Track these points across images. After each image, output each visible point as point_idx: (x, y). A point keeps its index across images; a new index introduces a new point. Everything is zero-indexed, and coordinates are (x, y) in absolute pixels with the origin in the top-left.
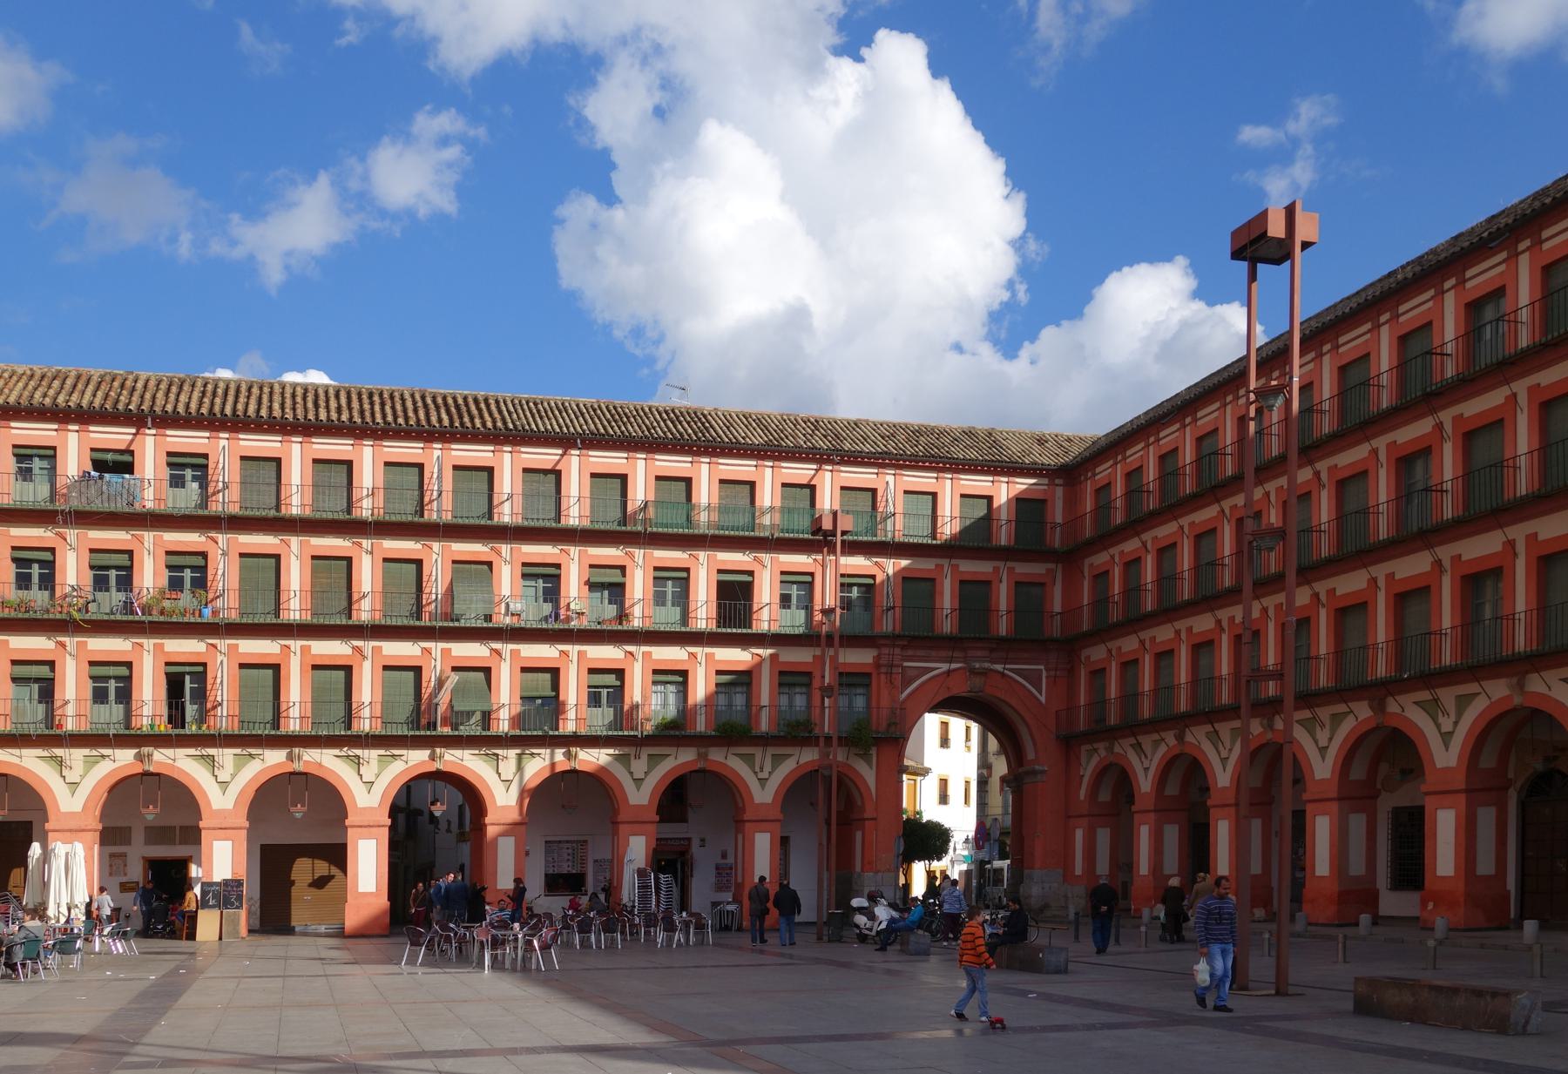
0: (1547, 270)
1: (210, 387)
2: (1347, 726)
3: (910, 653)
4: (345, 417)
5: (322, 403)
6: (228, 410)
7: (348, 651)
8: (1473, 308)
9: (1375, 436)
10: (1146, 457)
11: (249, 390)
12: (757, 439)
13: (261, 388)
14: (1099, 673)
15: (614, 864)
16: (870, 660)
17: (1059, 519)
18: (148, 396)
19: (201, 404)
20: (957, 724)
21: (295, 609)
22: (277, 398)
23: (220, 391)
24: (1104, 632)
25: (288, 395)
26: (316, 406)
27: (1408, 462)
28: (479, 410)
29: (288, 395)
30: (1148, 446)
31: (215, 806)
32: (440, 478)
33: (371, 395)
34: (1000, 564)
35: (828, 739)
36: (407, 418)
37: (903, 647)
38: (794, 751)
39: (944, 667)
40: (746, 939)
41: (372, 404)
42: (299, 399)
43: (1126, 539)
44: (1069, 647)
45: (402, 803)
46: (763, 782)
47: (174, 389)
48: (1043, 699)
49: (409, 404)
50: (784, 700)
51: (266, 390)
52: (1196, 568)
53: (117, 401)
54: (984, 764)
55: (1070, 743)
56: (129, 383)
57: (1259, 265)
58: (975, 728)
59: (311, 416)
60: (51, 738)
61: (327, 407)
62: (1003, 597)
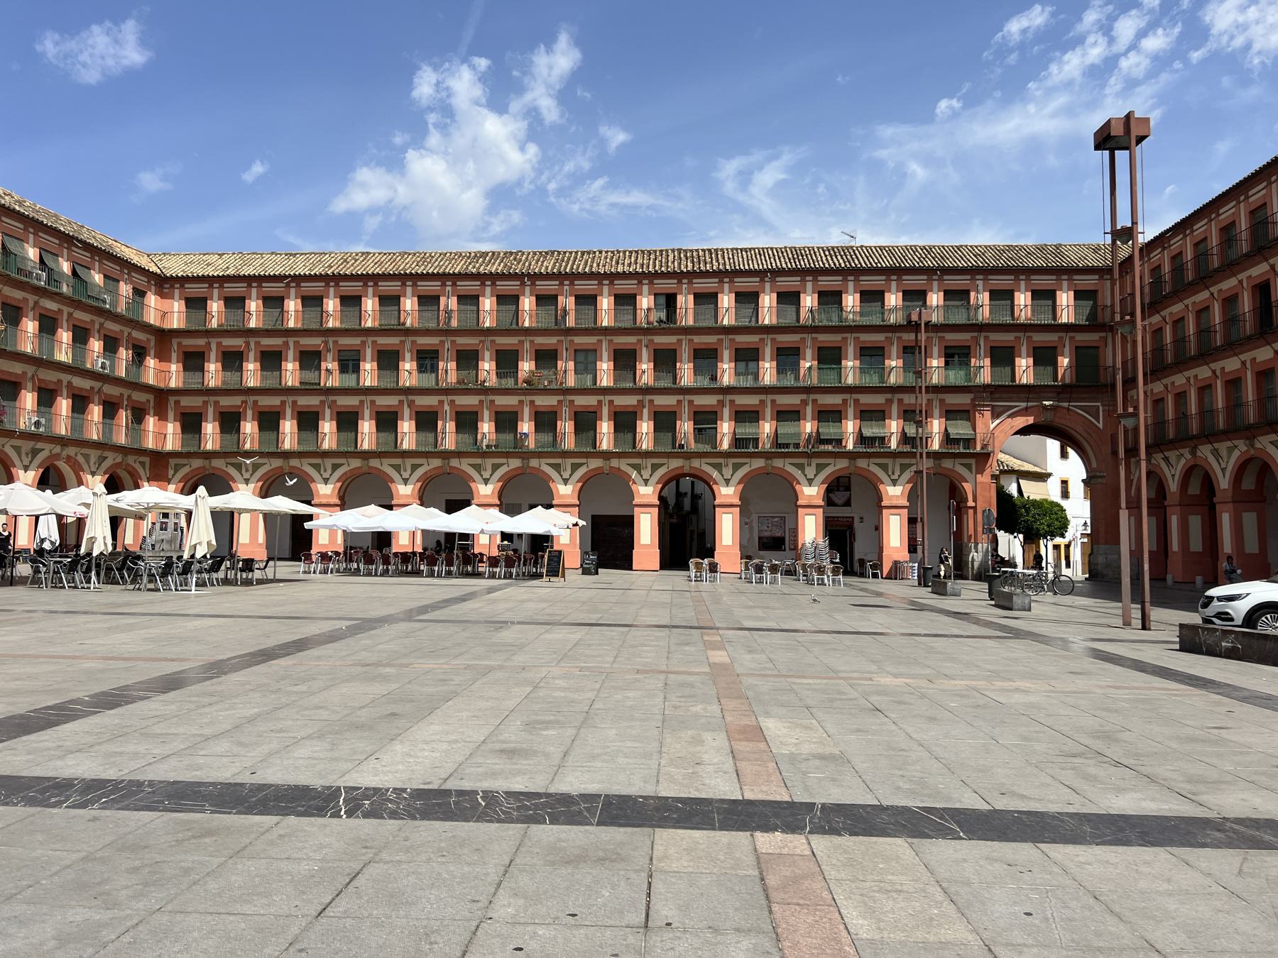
0: (1252, 213)
16: (969, 401)
27: (1230, 301)
30: (1185, 236)
39: (1024, 405)
40: (908, 589)
43: (1198, 292)
48: (1101, 426)
52: (1175, 342)
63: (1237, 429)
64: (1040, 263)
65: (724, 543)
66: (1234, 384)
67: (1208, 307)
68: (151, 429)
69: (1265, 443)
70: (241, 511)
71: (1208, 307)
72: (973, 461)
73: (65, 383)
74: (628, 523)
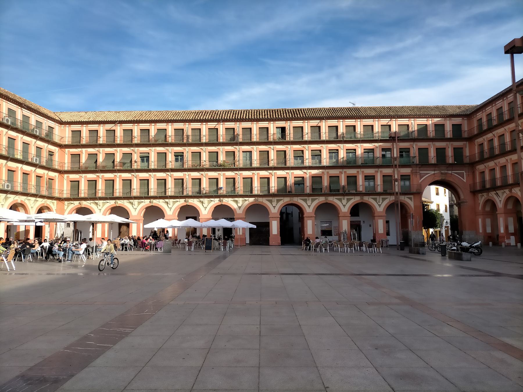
6: (239, 117)
7: (234, 174)
10: (493, 110)
12: (373, 114)
14: (483, 173)
15: (339, 227)
20: (441, 189)
22: (250, 113)
24: (483, 160)
28: (299, 112)
31: (238, 212)
32: (290, 130)
33: (272, 111)
34: (448, 143)
35: (397, 193)
36: (281, 116)
37: (419, 167)
38: (389, 197)
39: (433, 172)
41: (273, 113)
44: (472, 165)
45: (284, 211)
46: (380, 205)
48: (465, 181)
50: (367, 183)
54: (451, 200)
55: (474, 192)
57: (515, 55)
58: (447, 190)
60: (164, 197)
63: (505, 186)
65: (382, 220)
66: (492, 170)
67: (503, 135)
68: (57, 188)
69: (517, 192)
70: (97, 222)
71: (503, 135)
73: (19, 168)
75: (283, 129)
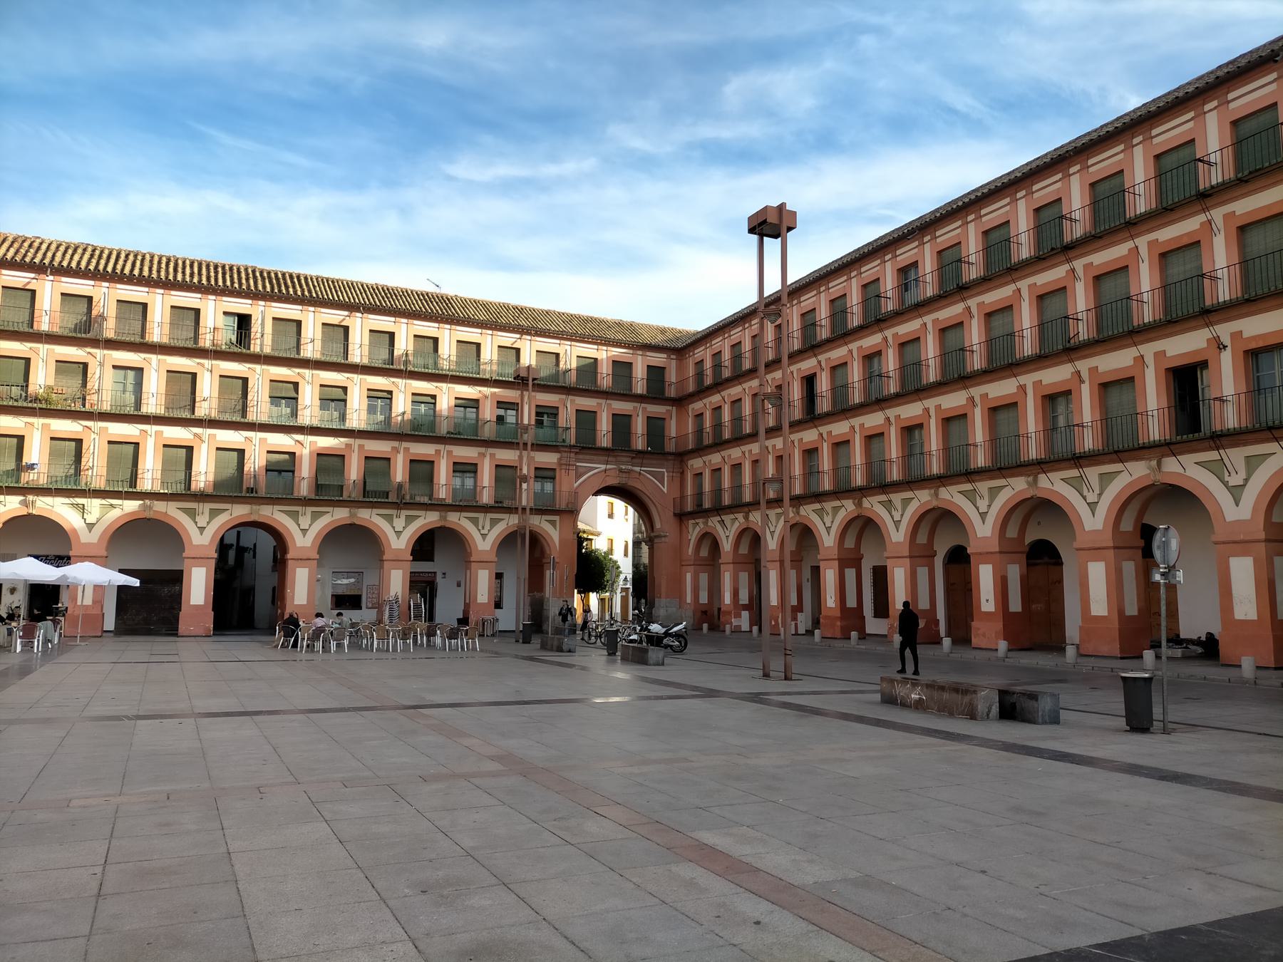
1: (97, 253)
2: (842, 514)
3: (581, 457)
4: (195, 280)
5: (180, 270)
8: (904, 271)
9: (851, 342)
10: (723, 345)
11: (127, 256)
12: (482, 316)
13: (136, 256)
14: (699, 475)
17: (674, 380)
18: (49, 255)
19: (89, 263)
20: (619, 505)
21: (152, 405)
23: (105, 256)
25: (156, 262)
26: (175, 270)
27: (871, 358)
29: (156, 262)
33: (216, 267)
35: (524, 509)
36: (240, 284)
38: (505, 516)
39: (603, 467)
41: (216, 273)
42: (163, 266)
44: (681, 457)
46: (484, 536)
47: (70, 252)
49: (243, 275)
51: (140, 258)
53: (25, 255)
55: (682, 517)
56: (36, 245)
59: (171, 277)
61: (184, 273)
62: (639, 426)
64: (620, 336)
65: (203, 570)
72: (557, 518)
74: (176, 578)
75: (244, 321)
